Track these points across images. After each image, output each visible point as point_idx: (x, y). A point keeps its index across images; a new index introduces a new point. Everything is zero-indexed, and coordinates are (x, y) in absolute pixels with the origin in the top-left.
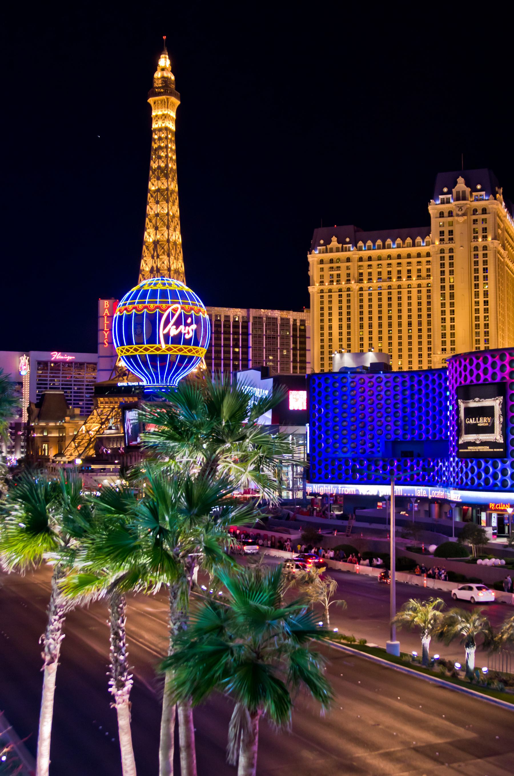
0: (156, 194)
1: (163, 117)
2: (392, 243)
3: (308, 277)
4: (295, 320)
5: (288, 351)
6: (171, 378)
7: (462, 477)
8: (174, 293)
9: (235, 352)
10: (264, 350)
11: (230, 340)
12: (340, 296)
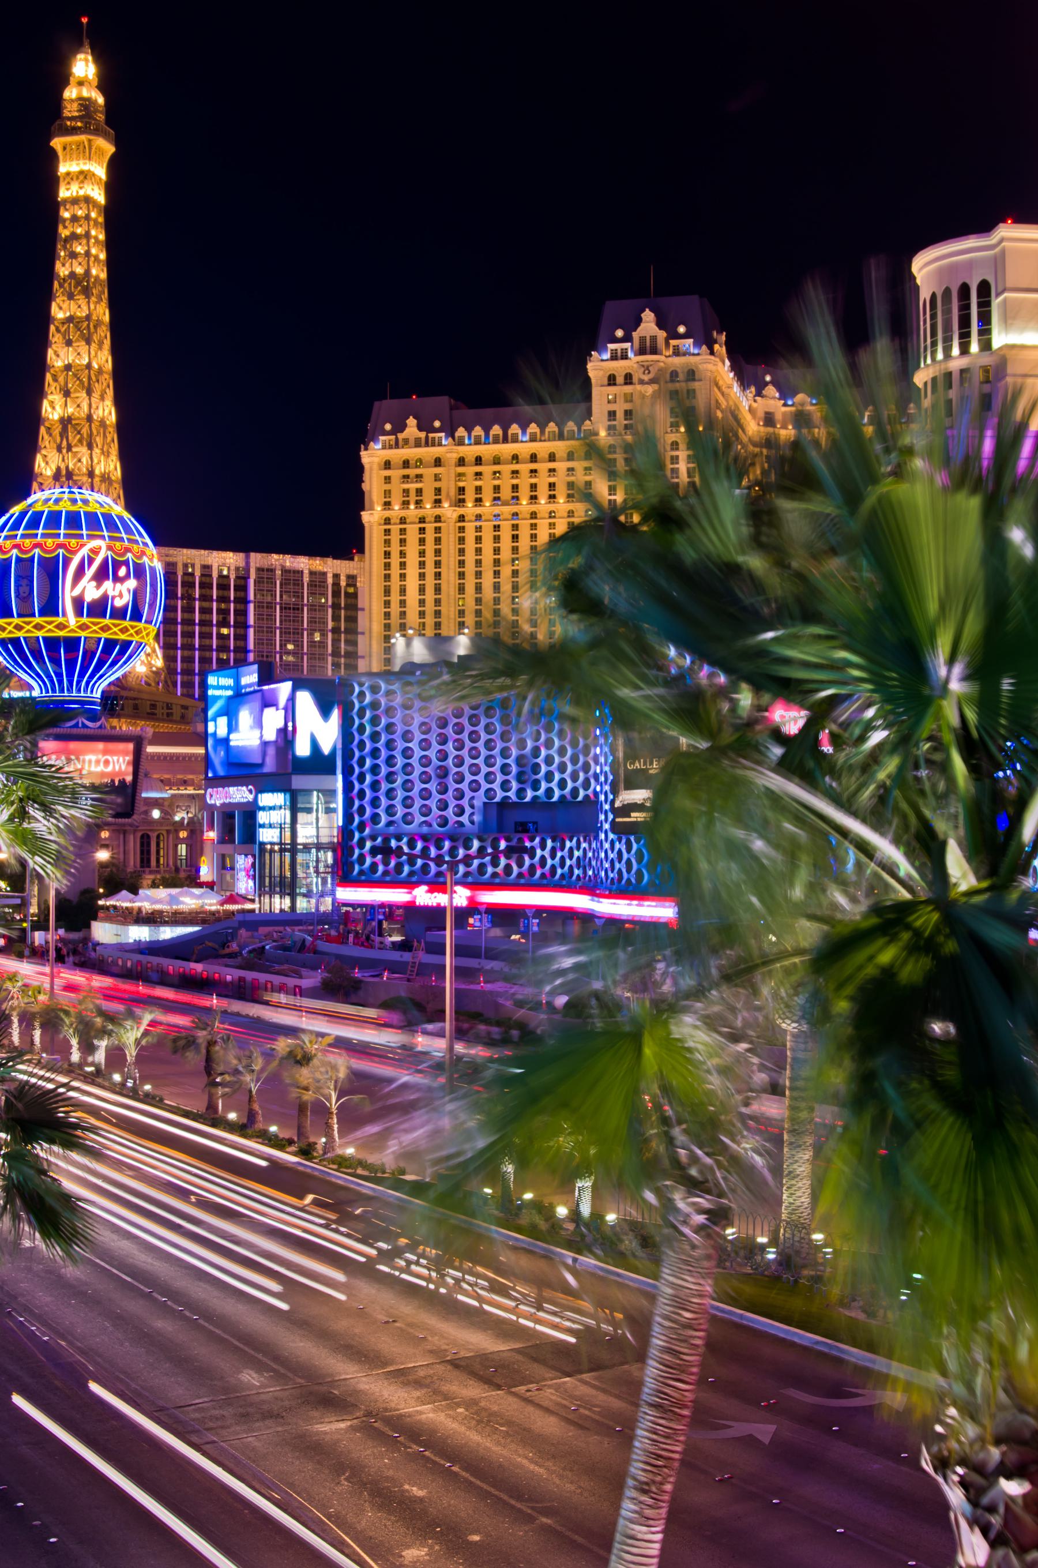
0: (66, 326)
1: (81, 177)
2: (520, 432)
3: (361, 494)
4: (336, 576)
5: (323, 635)
6: (88, 683)
7: (620, 870)
8: (93, 520)
9: (220, 636)
10: (278, 631)
11: (212, 613)
12: (422, 530)
